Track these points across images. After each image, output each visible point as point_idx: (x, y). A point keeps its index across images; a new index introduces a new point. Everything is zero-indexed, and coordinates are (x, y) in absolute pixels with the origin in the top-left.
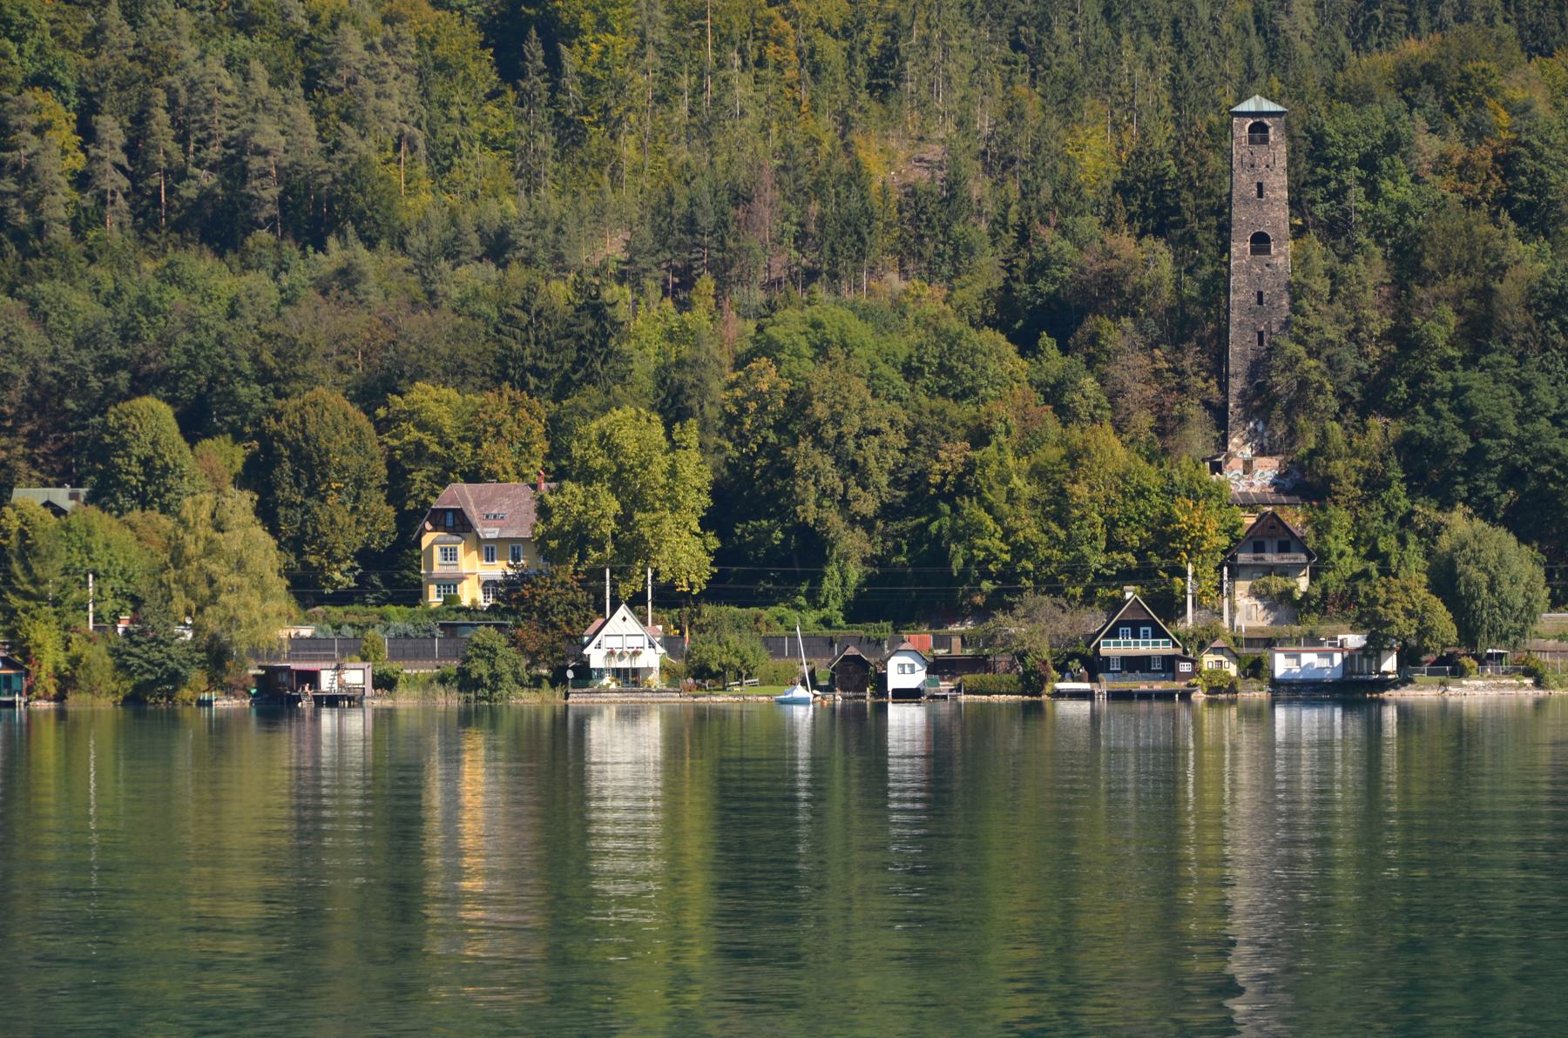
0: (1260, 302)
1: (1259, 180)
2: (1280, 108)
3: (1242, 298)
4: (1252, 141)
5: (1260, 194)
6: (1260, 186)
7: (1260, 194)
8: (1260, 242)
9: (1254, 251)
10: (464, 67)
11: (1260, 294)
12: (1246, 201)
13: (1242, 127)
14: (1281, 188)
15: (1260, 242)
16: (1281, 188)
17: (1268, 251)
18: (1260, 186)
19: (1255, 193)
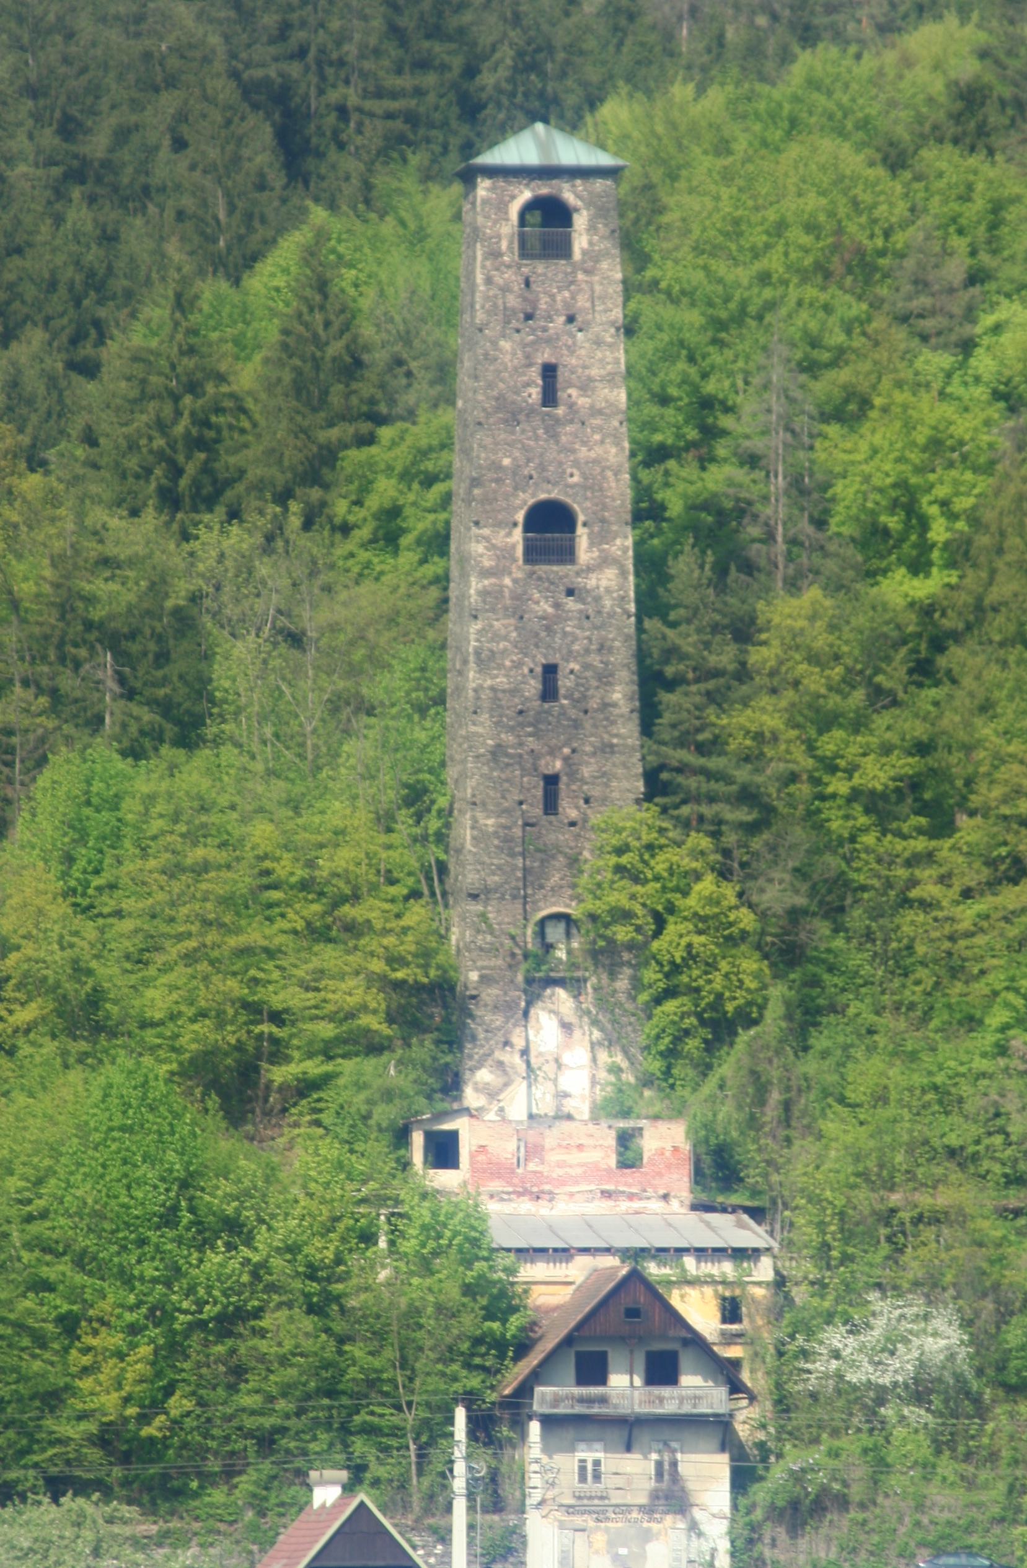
0: (549, 693)
1: (545, 356)
2: (604, 159)
3: (501, 681)
4: (526, 250)
5: (550, 396)
6: (549, 372)
7: (550, 396)
8: (550, 525)
9: (533, 554)
10: (464, 761)
11: (550, 670)
12: (513, 415)
13: (502, 207)
14: (610, 380)
15: (550, 525)
16: (610, 380)
17: (567, 554)
18: (549, 372)
19: (535, 394)
